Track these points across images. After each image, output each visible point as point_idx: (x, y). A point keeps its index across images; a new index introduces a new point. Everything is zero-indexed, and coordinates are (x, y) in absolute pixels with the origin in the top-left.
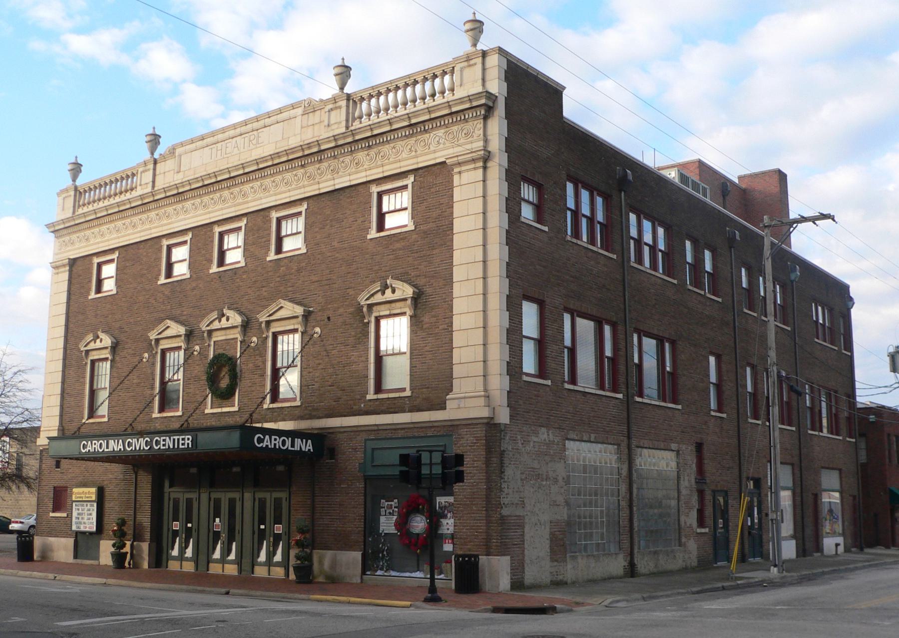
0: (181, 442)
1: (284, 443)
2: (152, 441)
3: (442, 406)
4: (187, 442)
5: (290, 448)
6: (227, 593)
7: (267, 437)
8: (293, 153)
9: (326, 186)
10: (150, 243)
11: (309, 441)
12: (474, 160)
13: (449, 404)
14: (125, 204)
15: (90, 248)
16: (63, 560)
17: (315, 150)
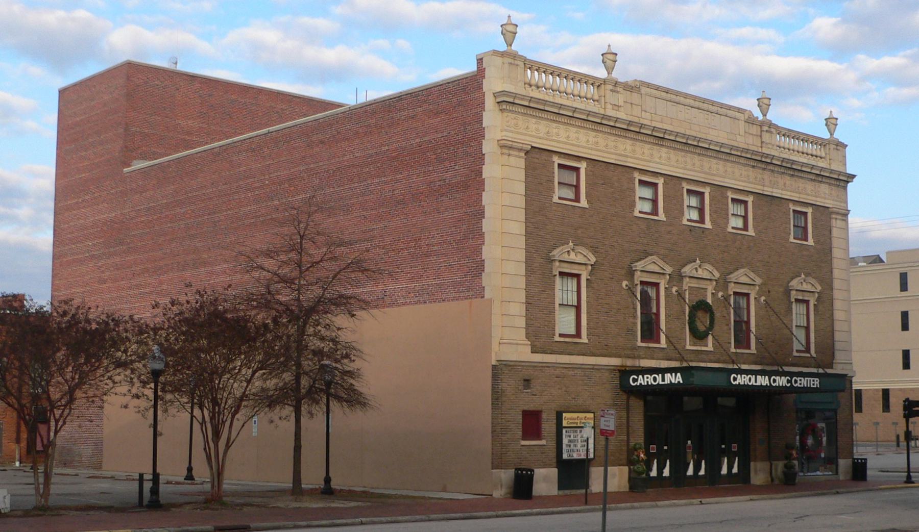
3: (831, 366)
6: (838, 493)
9: (768, 191)
10: (620, 169)
11: (679, 374)
12: (521, 150)
13: (835, 366)
14: (609, 120)
15: (606, 155)
16: (544, 494)
17: (769, 161)
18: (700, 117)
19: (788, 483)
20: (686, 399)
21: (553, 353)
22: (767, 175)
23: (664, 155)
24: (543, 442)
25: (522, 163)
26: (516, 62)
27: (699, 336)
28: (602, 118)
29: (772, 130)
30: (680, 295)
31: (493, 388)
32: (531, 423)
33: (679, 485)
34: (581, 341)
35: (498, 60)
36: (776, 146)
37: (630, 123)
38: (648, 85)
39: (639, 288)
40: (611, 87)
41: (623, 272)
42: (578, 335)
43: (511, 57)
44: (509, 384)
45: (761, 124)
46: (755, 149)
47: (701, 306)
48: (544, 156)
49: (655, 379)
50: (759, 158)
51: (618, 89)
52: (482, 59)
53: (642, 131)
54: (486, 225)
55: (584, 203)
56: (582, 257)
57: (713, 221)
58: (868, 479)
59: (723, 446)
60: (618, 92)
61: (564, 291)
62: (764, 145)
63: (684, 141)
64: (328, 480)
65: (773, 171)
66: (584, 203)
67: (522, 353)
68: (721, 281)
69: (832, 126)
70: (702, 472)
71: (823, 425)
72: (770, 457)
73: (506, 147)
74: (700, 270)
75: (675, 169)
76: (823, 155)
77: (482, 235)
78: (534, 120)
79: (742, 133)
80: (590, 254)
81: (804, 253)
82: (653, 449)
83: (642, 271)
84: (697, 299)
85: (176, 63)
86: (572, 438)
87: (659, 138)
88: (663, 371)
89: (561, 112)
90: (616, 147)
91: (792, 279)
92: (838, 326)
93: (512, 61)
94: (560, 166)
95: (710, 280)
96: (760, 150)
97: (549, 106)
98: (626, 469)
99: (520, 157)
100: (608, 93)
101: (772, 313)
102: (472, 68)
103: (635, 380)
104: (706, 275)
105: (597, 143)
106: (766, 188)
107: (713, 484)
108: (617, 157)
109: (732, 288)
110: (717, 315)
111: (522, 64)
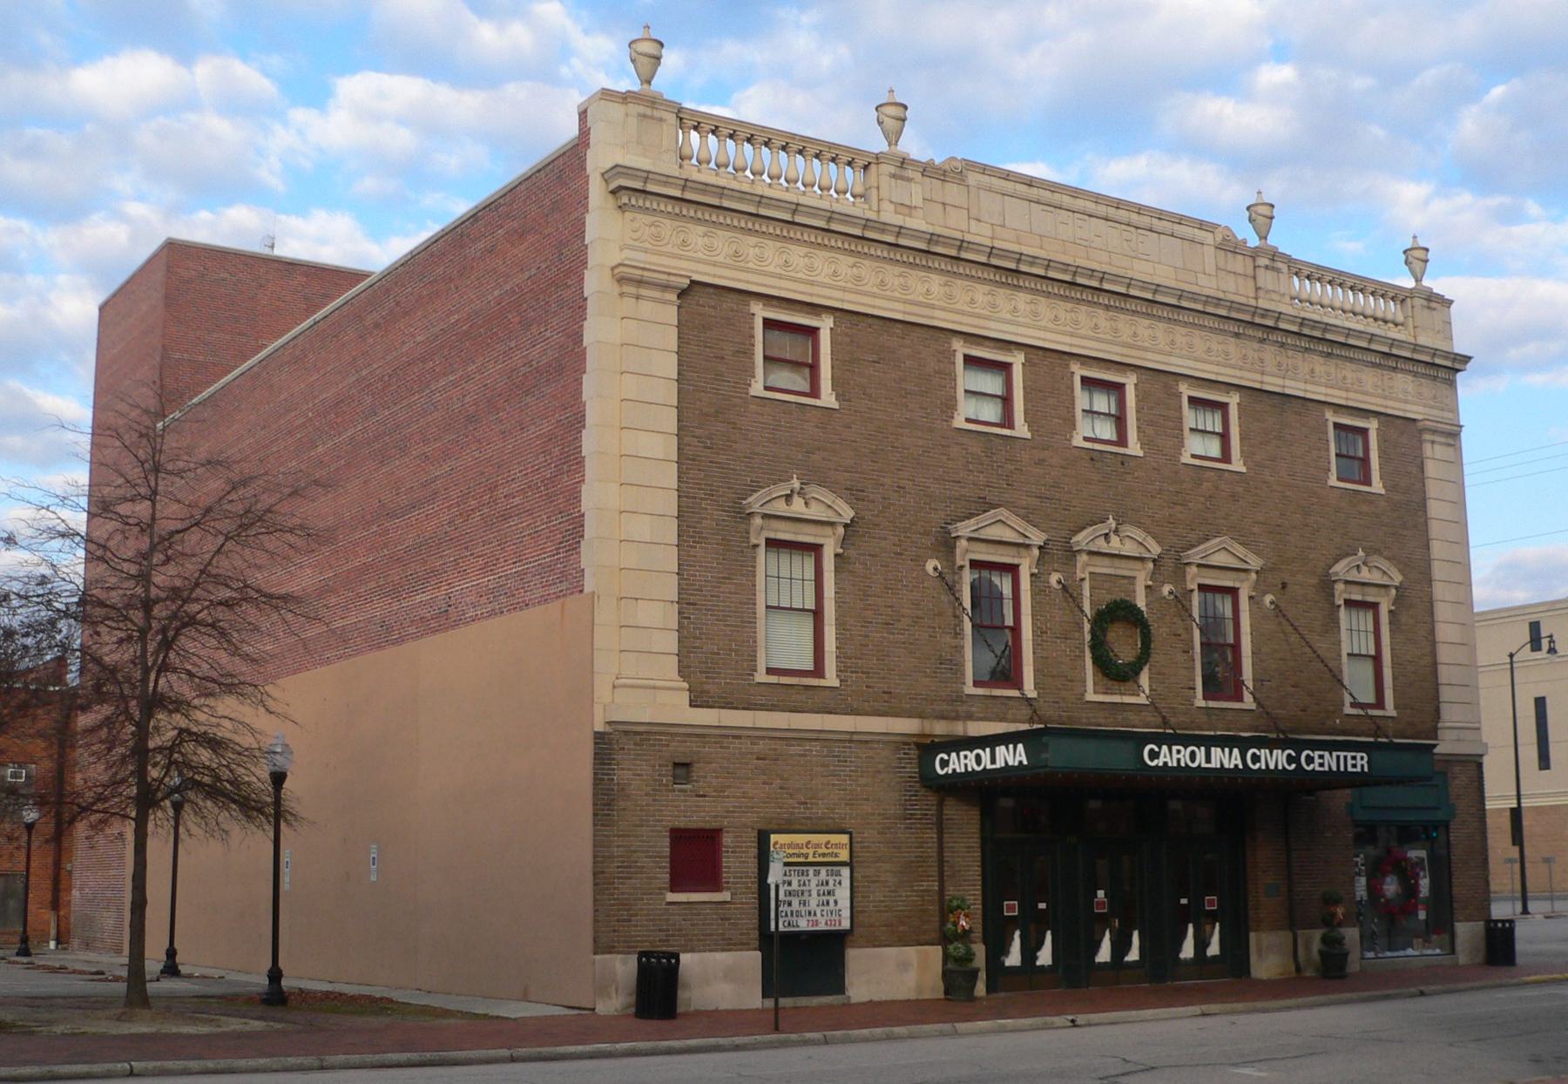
0: (1350, 762)
1: (1193, 756)
2: (1299, 756)
4: (1359, 763)
5: (1204, 765)
6: (1422, 994)
7: (1165, 748)
8: (1238, 310)
9: (1273, 384)
10: (898, 329)
11: (1020, 746)
12: (666, 287)
14: (883, 231)
15: (878, 302)
16: (724, 1006)
17: (1270, 323)
18: (1113, 236)
19: (1329, 974)
20: (1175, 805)
21: (749, 707)
22: (1270, 353)
23: (1021, 306)
24: (725, 896)
25: (671, 314)
26: (657, 114)
27: (1115, 673)
28: (865, 227)
29: (1279, 265)
30: (1069, 592)
31: (597, 781)
32: (695, 856)
33: (1020, 990)
34: (822, 682)
35: (616, 111)
36: (1290, 297)
37: (933, 238)
38: (985, 169)
39: (967, 577)
40: (892, 170)
41: (928, 541)
42: (818, 671)
43: (646, 104)
44: (633, 773)
45: (1254, 254)
46: (1243, 300)
47: (1118, 613)
48: (730, 302)
49: (978, 759)
50: (1247, 318)
51: (910, 173)
52: (585, 112)
53: (964, 255)
54: (590, 442)
55: (828, 398)
56: (823, 508)
57: (1144, 441)
58: (1519, 960)
59: (1184, 901)
60: (909, 180)
61: (781, 582)
62: (1261, 293)
63: (1067, 278)
64: (275, 975)
65: (1283, 345)
66: (828, 398)
67: (670, 705)
68: (1169, 563)
69: (1418, 265)
70: (1133, 955)
71: (1423, 854)
72: (1293, 921)
73: (631, 280)
74: (1115, 540)
75: (1048, 335)
76: (1400, 318)
77: (580, 462)
78: (701, 229)
79: (1211, 269)
80: (840, 502)
81: (1364, 508)
82: (1011, 908)
83: (970, 539)
84: (1108, 598)
85: (272, 247)
86: (795, 886)
87: (1009, 272)
88: (991, 742)
89: (762, 212)
90: (905, 288)
91: (1336, 561)
92: (1444, 654)
93: (649, 111)
94: (768, 323)
95: (1141, 559)
96: (1252, 302)
97: (731, 198)
98: (936, 952)
99: (665, 302)
100: (885, 181)
101: (1290, 629)
102: (571, 130)
103: (944, 763)
104: (1129, 549)
105: (858, 279)
106: (1267, 379)
107: (1160, 979)
108: (909, 308)
109: (1194, 578)
110: (1159, 631)
111: (672, 119)
